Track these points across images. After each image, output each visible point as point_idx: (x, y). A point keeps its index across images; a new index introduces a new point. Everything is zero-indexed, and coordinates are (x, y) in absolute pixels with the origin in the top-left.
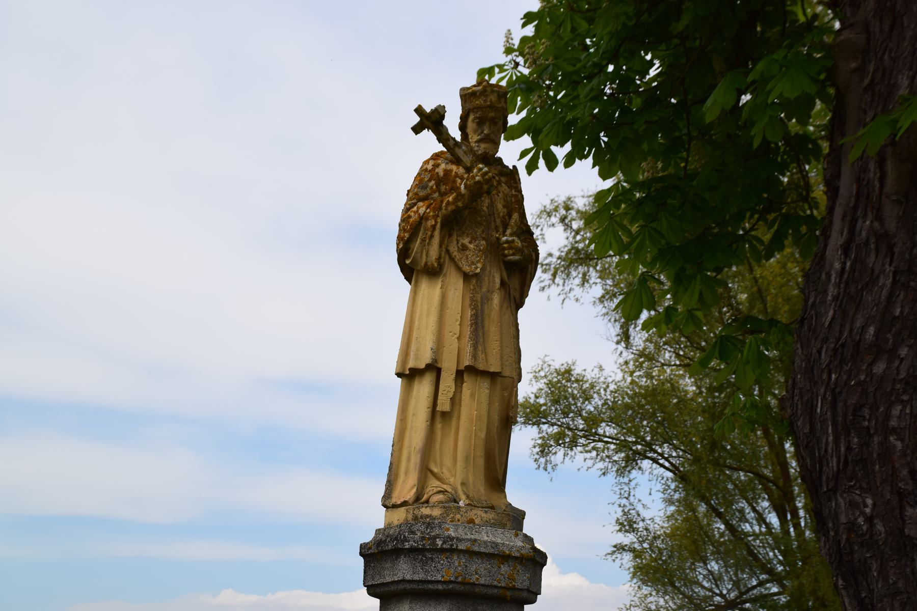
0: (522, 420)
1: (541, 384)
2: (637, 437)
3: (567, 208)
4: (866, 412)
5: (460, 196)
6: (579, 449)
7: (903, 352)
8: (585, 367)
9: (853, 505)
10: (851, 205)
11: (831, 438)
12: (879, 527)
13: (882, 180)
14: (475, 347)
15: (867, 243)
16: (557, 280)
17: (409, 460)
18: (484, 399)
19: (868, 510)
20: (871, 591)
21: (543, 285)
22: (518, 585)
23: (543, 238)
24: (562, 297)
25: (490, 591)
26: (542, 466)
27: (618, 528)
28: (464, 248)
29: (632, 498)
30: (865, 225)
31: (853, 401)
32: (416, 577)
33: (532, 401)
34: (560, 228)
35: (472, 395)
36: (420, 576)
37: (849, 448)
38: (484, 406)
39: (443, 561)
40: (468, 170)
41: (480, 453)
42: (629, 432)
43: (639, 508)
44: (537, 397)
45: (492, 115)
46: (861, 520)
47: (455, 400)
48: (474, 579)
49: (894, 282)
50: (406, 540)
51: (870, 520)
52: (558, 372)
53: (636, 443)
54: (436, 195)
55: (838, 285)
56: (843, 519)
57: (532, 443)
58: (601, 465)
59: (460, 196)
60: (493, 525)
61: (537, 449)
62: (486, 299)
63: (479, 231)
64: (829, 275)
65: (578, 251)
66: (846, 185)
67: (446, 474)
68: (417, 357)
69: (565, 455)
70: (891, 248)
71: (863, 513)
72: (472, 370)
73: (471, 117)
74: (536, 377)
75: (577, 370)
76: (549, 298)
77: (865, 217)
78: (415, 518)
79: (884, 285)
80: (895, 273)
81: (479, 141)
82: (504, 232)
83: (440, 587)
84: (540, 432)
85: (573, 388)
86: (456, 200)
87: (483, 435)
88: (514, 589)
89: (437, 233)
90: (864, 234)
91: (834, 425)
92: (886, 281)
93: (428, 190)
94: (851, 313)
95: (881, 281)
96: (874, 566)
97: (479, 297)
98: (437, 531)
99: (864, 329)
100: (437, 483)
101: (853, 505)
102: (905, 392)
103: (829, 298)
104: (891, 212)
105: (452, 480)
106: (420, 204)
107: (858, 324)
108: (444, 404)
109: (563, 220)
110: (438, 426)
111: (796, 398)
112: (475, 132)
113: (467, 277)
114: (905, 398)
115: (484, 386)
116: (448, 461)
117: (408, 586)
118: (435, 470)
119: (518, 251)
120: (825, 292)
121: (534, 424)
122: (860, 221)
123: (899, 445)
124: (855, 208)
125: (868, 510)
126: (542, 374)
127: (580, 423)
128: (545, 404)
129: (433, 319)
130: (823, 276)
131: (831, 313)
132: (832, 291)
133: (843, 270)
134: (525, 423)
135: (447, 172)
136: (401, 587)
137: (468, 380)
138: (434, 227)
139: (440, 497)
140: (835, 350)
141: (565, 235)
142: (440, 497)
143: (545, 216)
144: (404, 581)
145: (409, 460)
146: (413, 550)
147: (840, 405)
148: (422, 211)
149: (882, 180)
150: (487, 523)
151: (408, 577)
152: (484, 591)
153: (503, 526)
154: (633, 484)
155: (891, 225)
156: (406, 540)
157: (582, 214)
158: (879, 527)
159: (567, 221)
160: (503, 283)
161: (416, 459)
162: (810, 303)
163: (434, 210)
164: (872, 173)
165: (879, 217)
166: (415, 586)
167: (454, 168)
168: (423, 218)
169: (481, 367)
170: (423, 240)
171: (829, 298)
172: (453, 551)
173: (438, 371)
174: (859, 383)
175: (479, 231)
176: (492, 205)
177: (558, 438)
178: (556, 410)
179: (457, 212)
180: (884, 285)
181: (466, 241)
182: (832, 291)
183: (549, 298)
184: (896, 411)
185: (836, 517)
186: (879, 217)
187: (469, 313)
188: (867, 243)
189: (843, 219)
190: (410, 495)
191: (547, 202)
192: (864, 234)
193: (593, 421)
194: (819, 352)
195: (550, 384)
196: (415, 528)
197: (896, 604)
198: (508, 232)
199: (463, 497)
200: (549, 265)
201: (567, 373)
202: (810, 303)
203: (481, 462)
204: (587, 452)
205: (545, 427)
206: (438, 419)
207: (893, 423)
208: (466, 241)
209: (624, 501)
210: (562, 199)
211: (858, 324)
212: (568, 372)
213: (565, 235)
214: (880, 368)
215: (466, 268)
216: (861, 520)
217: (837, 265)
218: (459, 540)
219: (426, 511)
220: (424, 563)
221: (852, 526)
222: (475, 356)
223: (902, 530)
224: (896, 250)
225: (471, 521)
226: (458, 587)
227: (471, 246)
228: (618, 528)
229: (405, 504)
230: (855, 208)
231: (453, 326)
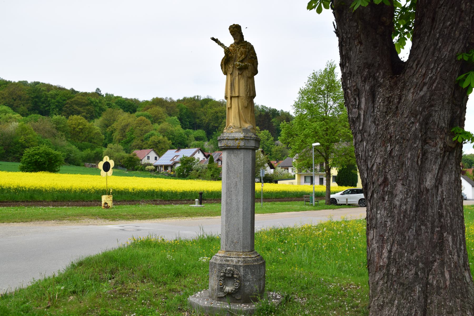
7: (347, 64)
88: (240, 146)
226: (226, 147)
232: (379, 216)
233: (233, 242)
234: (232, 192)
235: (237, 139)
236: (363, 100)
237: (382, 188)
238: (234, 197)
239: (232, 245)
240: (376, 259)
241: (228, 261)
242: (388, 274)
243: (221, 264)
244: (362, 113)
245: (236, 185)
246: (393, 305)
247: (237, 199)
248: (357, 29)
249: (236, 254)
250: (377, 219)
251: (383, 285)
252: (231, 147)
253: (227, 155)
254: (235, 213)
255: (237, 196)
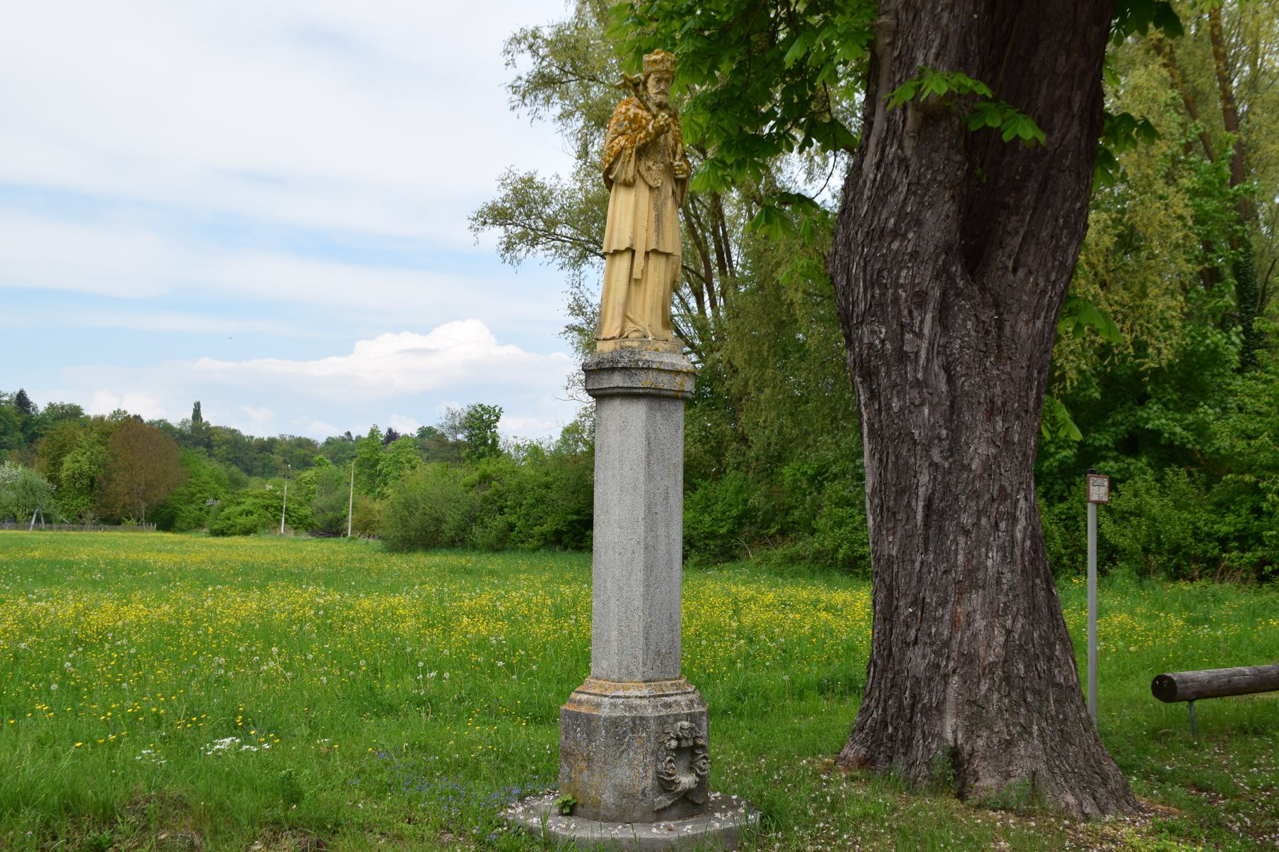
0: (491, 221)
1: (508, 191)
2: (590, 237)
3: (535, 37)
4: (885, 273)
5: (648, 134)
6: (540, 247)
7: (911, 235)
8: (545, 176)
9: (873, 332)
10: (883, 136)
11: (861, 290)
12: (888, 346)
13: (904, 122)
14: (658, 236)
15: (892, 163)
16: (527, 101)
17: (614, 309)
18: (662, 271)
19: (882, 336)
20: (879, 385)
21: (513, 104)
22: (686, 389)
23: (514, 63)
24: (531, 116)
25: (669, 393)
26: (507, 261)
27: (569, 312)
28: (649, 169)
29: (582, 287)
30: (892, 151)
31: (877, 266)
32: (626, 385)
33: (500, 205)
34: (528, 54)
35: (655, 268)
36: (629, 384)
37: (873, 297)
38: (663, 276)
39: (642, 375)
40: (655, 117)
41: (660, 305)
42: (583, 233)
43: (588, 295)
44: (504, 202)
45: (667, 76)
46: (877, 342)
47: (644, 272)
48: (660, 386)
49: (908, 190)
50: (619, 362)
51: (883, 342)
52: (522, 180)
53: (588, 242)
54: (629, 131)
55: (871, 189)
56: (866, 341)
57: (499, 241)
58: (559, 260)
59: (648, 134)
60: (670, 352)
61: (503, 246)
62: (664, 204)
63: (659, 157)
64: (865, 182)
65: (543, 76)
66: (879, 120)
67: (638, 319)
68: (619, 242)
69: (528, 251)
70: (907, 167)
71: (879, 337)
72: (655, 252)
73: (652, 76)
74: (503, 184)
75: (538, 179)
76: (518, 117)
77: (892, 145)
78: (622, 348)
79: (901, 192)
80: (909, 184)
81: (657, 93)
82: (674, 158)
83: (641, 391)
84: (507, 231)
85: (534, 194)
86: (646, 136)
87: (661, 294)
88: (683, 391)
89: (633, 159)
90: (890, 156)
91: (865, 281)
92: (903, 189)
93: (624, 128)
94: (880, 209)
95: (900, 189)
96: (883, 370)
97: (659, 203)
98: (637, 357)
99: (887, 220)
100: (632, 325)
101: (873, 332)
102: (910, 261)
103: (865, 197)
104: (909, 144)
105: (642, 323)
106: (620, 138)
107: (884, 217)
108: (637, 274)
109: (530, 47)
110: (633, 288)
111: (837, 262)
112: (654, 87)
113: (651, 188)
114: (910, 265)
115: (662, 260)
116: (639, 311)
117: (620, 390)
118: (631, 316)
119: (685, 172)
120: (862, 193)
121: (501, 225)
122: (888, 148)
123: (904, 294)
124: (886, 139)
125: (882, 336)
126: (509, 181)
127: (541, 224)
128: (510, 208)
129: (630, 217)
130: (861, 181)
131: (866, 208)
132: (867, 193)
133: (875, 178)
134: (493, 224)
135: (636, 115)
136: (615, 391)
137: (652, 257)
138: (631, 155)
139: (636, 334)
140: (868, 233)
141: (532, 61)
142: (636, 334)
143: (515, 42)
144: (618, 387)
145: (614, 309)
146: (623, 368)
147: (869, 268)
148: (622, 143)
149: (904, 122)
150: (666, 351)
151: (621, 385)
152: (666, 393)
153: (675, 352)
154: (583, 275)
155: (909, 152)
156: (619, 362)
157: (548, 43)
158: (888, 346)
159: (534, 48)
160: (673, 192)
161: (619, 310)
162: (850, 198)
163: (631, 143)
164: (898, 116)
165: (901, 147)
166: (625, 391)
167: (640, 111)
168: (623, 148)
169: (661, 250)
170: (623, 163)
171: (865, 197)
172: (649, 368)
173: (633, 252)
174: (882, 255)
175: (659, 157)
176: (666, 138)
177: (522, 237)
178: (520, 213)
179: (646, 145)
180: (901, 192)
181: (650, 164)
182: (867, 193)
183: (518, 117)
184: (904, 273)
185: (861, 340)
186: (901, 147)
187: (654, 214)
188: (892, 163)
189: (877, 145)
190: (616, 333)
191: (517, 31)
192: (890, 156)
193: (552, 223)
194: (857, 233)
195: (515, 190)
196: (623, 354)
197: (895, 392)
198: (677, 158)
199: (650, 334)
200: (519, 87)
201: (529, 181)
202: (850, 198)
203: (660, 311)
204: (548, 249)
205: (510, 227)
206: (633, 283)
207: (901, 281)
208: (650, 164)
209: (575, 290)
210: (530, 28)
211: (884, 217)
212: (531, 180)
213: (532, 61)
214: (895, 246)
215: (651, 183)
216: (877, 342)
217: (871, 176)
218: (653, 362)
219: (628, 343)
220: (631, 377)
221: (871, 345)
222: (658, 243)
223: (901, 348)
224: (911, 169)
225: (657, 350)
226: (652, 391)
227: (654, 168)
228: (569, 312)
229: (613, 338)
230: (886, 139)
231: (643, 222)
232: (990, 562)
233: (658, 653)
234: (658, 516)
235: (678, 372)
236: (929, 317)
237: (996, 506)
238: (661, 531)
239: (658, 663)
240: (982, 652)
241: (668, 706)
242: (1007, 678)
243: (660, 717)
244: (924, 345)
245: (667, 498)
246: (1031, 734)
247: (668, 536)
248: (958, 170)
249: (672, 685)
250: (986, 567)
251: (1000, 700)
252: (662, 392)
253: (647, 413)
254: (665, 574)
255: (667, 526)
